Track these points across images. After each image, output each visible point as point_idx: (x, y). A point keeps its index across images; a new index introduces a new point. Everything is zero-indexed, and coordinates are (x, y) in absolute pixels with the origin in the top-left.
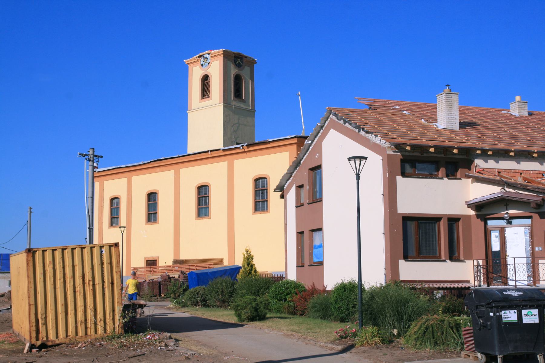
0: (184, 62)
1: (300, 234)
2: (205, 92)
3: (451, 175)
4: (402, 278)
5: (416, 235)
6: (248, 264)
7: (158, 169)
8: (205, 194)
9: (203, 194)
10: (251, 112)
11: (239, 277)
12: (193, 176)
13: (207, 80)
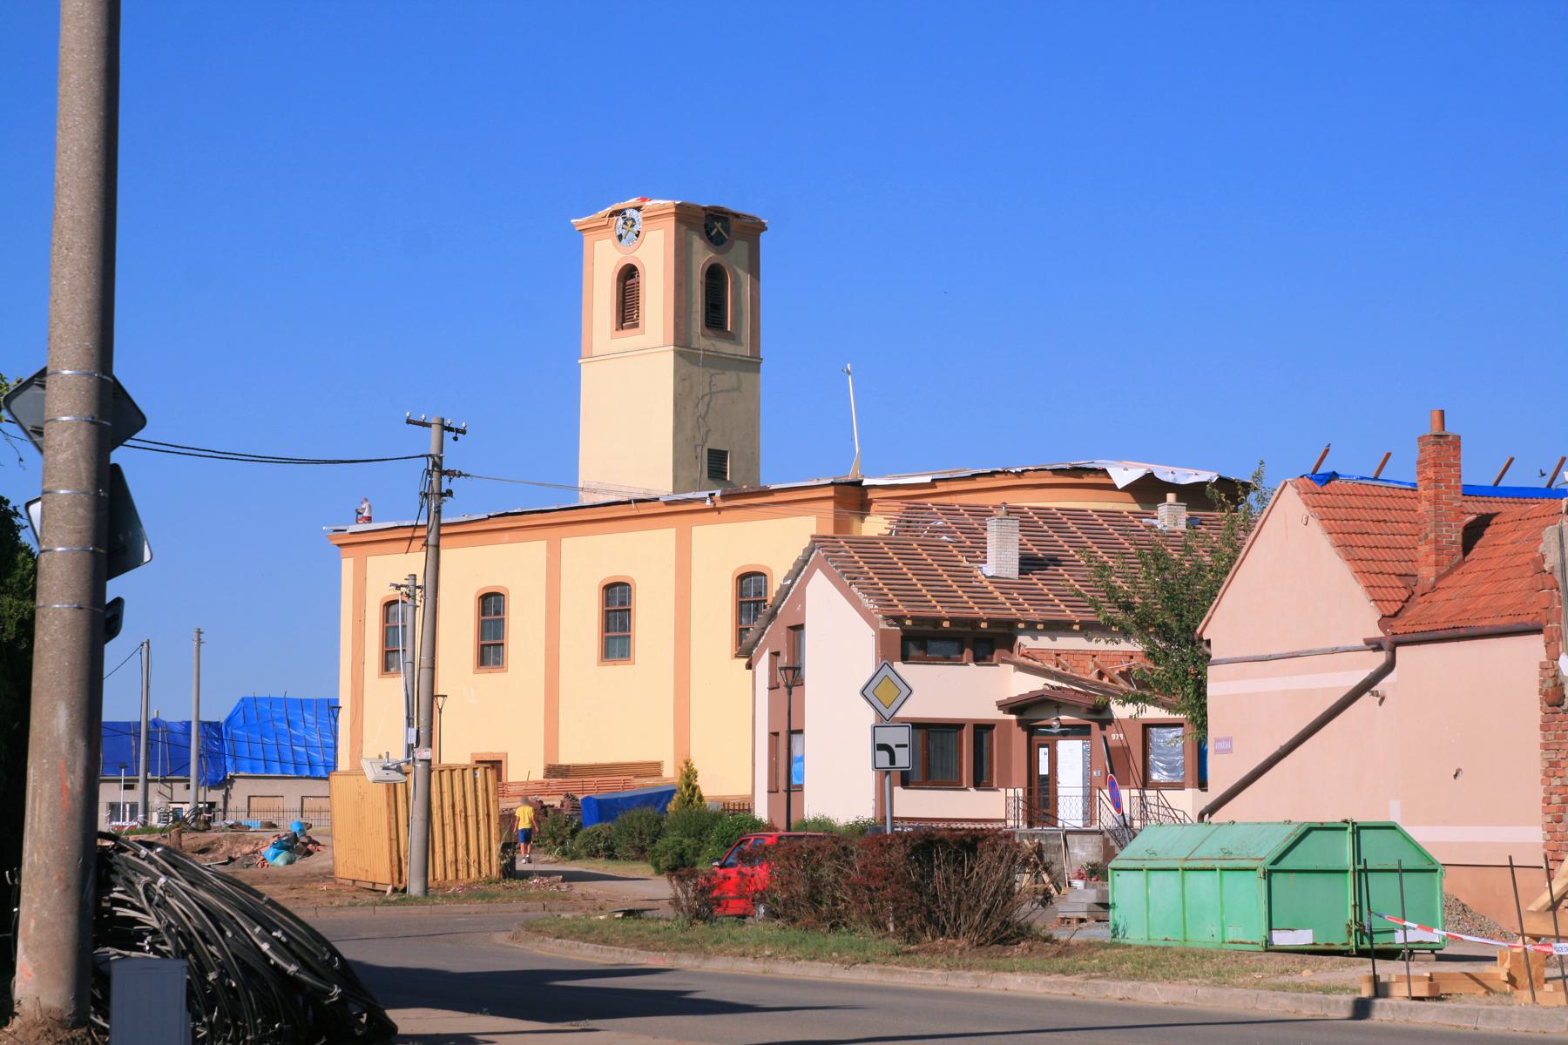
0: (573, 226)
1: (774, 734)
2: (627, 310)
3: (980, 659)
5: (937, 751)
6: (688, 786)
7: (507, 535)
8: (622, 603)
9: (617, 603)
10: (752, 364)
11: (671, 807)
12: (593, 557)
13: (633, 277)
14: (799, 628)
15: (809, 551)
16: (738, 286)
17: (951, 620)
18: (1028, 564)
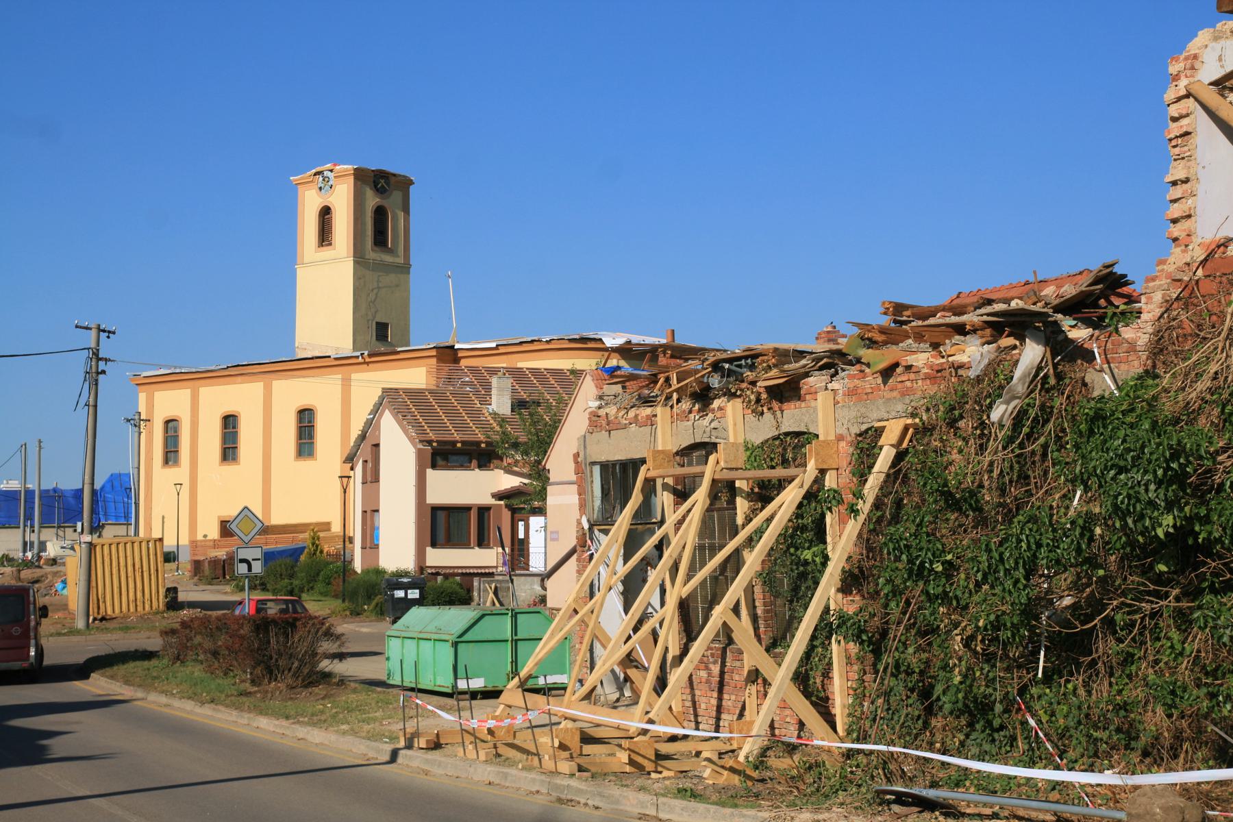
1: (364, 512)
3: (482, 466)
4: (428, 564)
5: (442, 524)
7: (239, 378)
8: (310, 422)
10: (405, 268)
11: (303, 558)
12: (293, 392)
14: (377, 446)
15: (382, 399)
16: (395, 221)
17: (463, 442)
18: (519, 405)
